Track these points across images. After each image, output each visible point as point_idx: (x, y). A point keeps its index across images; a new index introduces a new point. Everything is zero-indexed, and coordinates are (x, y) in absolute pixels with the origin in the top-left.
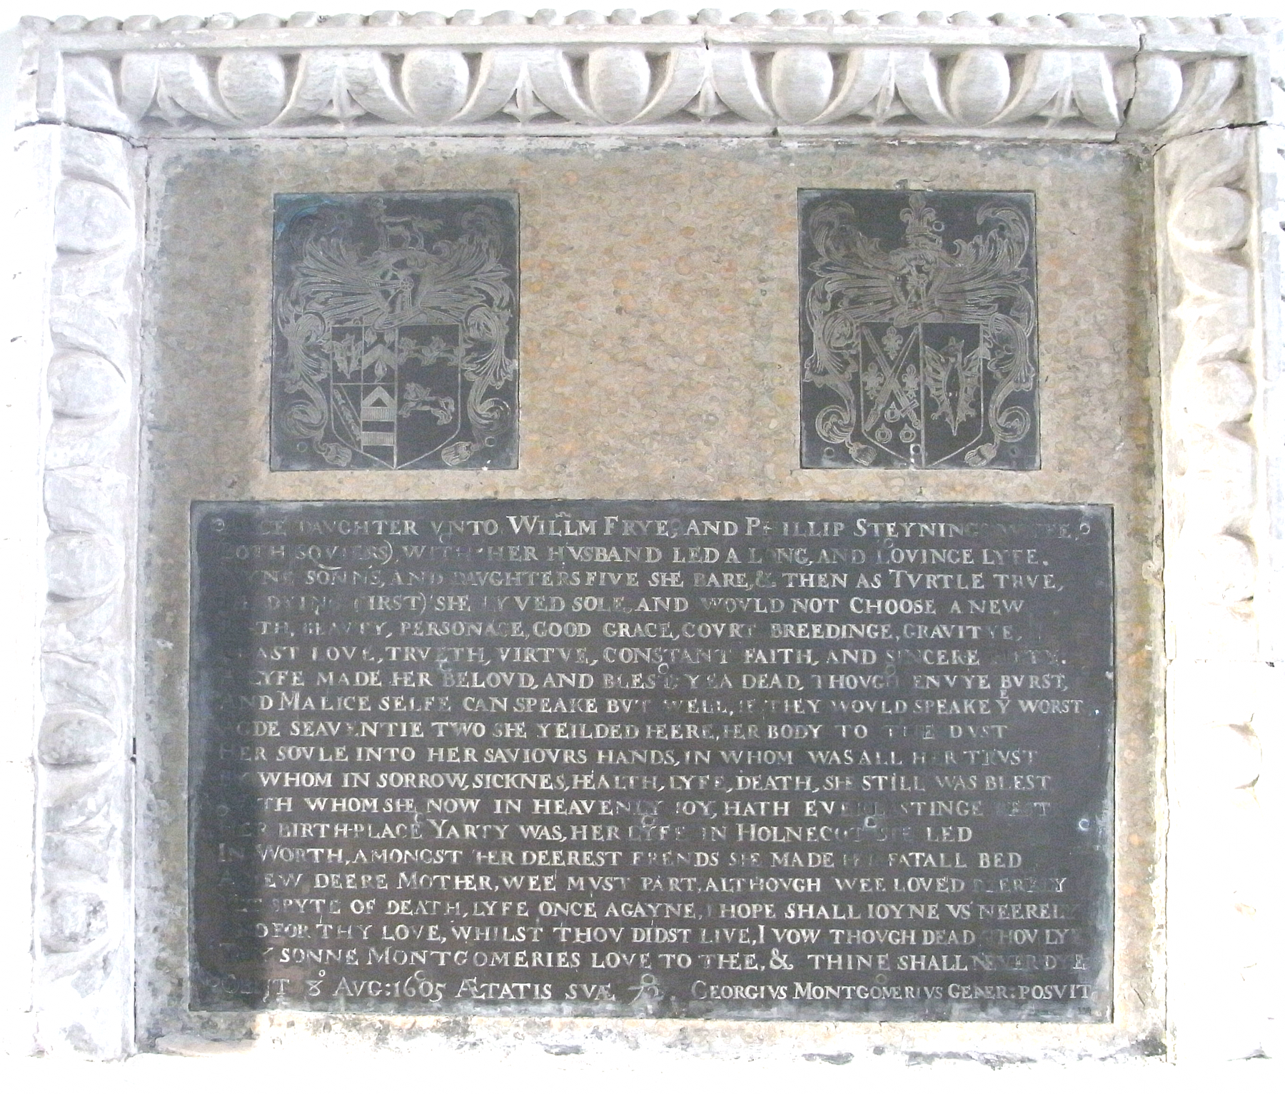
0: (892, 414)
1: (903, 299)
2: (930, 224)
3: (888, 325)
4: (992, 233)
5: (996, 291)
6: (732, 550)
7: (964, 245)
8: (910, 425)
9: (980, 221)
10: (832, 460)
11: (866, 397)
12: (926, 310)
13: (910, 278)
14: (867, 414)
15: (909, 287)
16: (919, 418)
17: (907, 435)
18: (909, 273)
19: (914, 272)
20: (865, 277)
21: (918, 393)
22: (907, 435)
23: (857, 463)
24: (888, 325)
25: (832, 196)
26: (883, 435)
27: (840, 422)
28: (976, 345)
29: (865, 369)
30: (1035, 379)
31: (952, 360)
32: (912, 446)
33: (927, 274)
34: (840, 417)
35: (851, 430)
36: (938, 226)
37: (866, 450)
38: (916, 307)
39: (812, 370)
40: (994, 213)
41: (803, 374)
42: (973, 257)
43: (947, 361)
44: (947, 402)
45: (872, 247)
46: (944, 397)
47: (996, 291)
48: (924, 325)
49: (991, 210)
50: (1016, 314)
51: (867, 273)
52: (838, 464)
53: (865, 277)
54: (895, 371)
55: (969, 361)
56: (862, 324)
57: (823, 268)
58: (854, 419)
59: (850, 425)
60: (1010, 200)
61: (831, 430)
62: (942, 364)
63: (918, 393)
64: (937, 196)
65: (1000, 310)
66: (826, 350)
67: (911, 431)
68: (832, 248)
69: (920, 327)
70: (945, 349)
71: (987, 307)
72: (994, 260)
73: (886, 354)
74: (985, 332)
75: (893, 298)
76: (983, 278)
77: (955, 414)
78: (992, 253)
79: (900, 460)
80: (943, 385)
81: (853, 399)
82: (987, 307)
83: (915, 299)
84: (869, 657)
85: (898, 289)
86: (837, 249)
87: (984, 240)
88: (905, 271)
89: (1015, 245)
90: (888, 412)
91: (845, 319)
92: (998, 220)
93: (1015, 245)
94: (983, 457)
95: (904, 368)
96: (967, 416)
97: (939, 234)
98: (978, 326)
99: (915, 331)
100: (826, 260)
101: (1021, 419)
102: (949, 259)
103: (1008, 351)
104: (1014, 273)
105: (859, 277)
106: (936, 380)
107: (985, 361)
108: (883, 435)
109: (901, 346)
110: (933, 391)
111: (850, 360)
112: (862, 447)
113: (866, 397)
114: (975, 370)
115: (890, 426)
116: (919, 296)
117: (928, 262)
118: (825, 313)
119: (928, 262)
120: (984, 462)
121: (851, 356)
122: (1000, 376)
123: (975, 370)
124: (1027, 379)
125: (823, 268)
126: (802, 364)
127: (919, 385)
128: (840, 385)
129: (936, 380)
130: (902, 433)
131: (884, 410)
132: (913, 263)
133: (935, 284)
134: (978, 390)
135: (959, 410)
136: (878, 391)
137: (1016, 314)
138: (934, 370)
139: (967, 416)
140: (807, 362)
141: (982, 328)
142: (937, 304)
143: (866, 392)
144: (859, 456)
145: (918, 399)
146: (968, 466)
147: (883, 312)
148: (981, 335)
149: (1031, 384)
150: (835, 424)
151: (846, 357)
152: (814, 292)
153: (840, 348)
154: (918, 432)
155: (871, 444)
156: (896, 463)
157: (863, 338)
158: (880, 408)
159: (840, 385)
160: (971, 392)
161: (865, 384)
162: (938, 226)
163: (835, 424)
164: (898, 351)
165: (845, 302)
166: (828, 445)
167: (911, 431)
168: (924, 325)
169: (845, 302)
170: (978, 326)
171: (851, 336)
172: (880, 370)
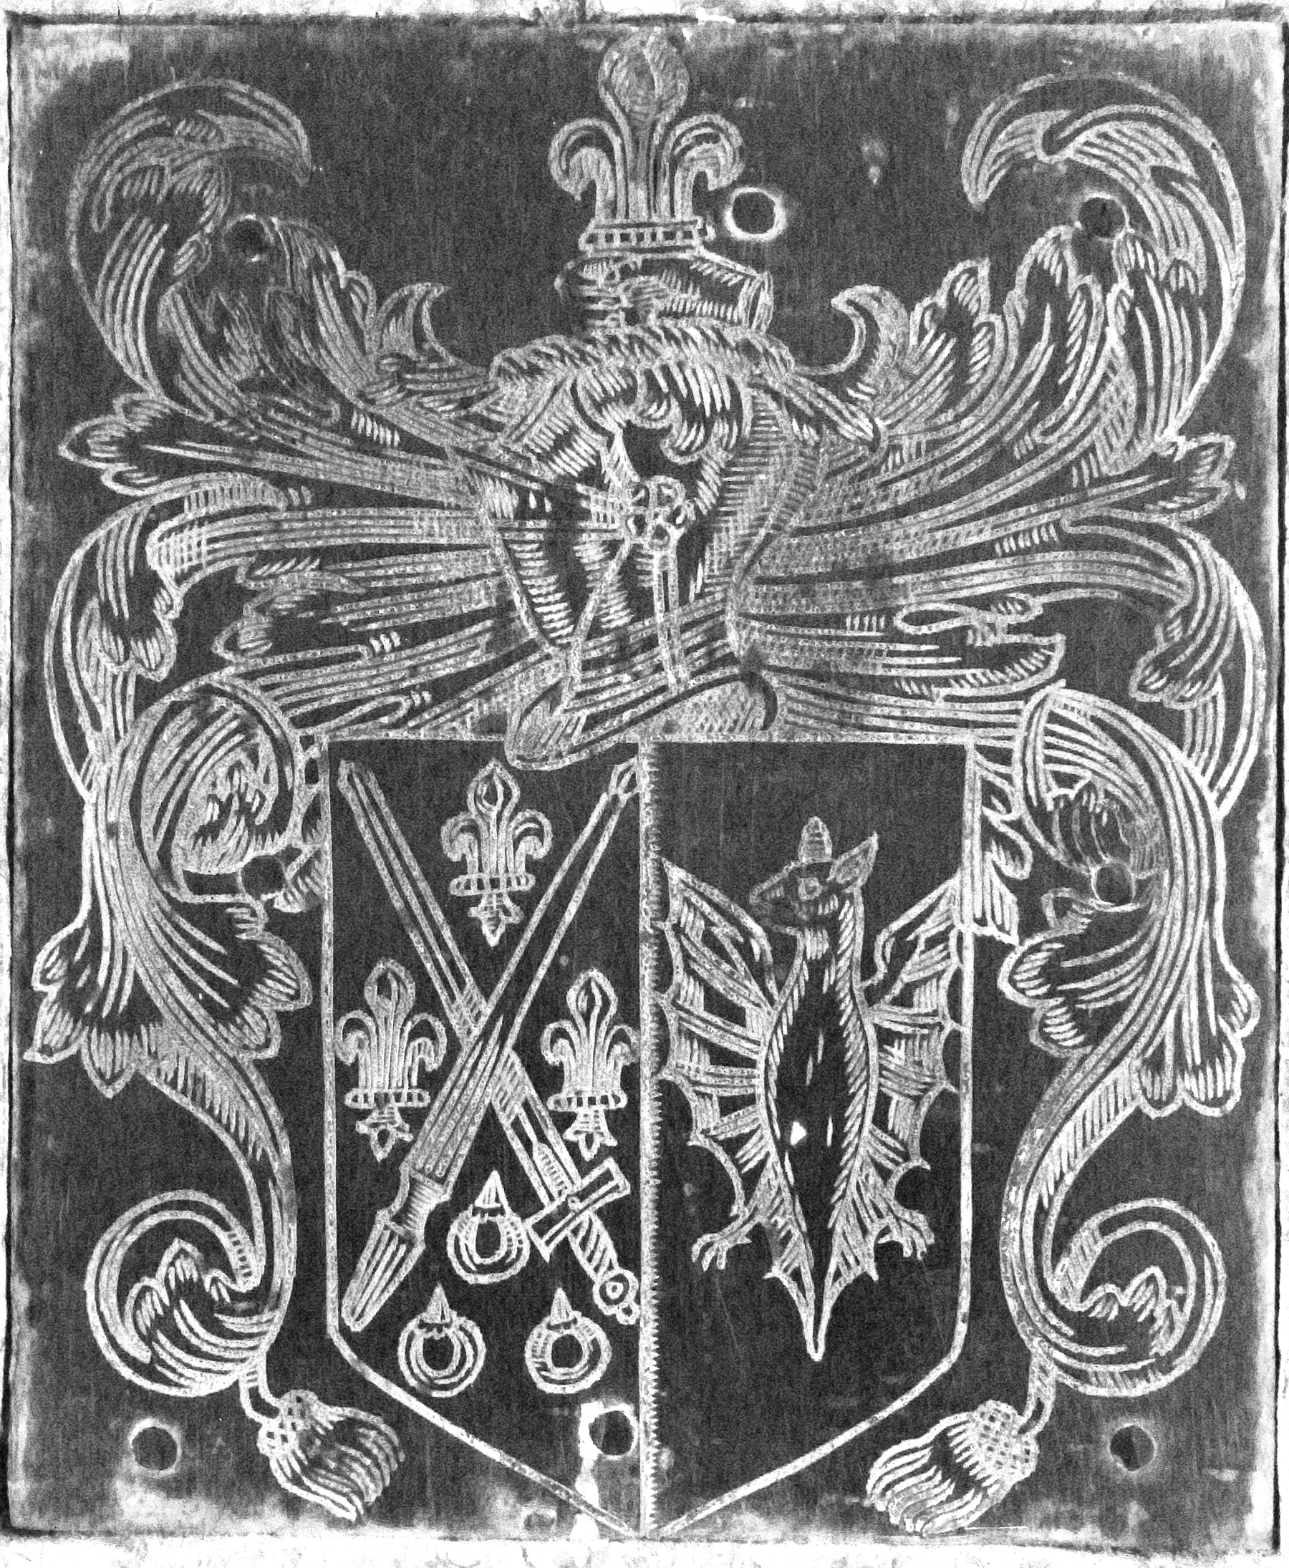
0: (488, 1239)
1: (556, 613)
2: (707, 202)
3: (474, 756)
4: (1042, 249)
5: (1059, 567)
6: (817, 1357)
7: (888, 315)
8: (581, 1301)
9: (978, 192)
10: (176, 1488)
11: (351, 1146)
12: (675, 676)
13: (594, 502)
14: (353, 1240)
15: (589, 551)
16: (629, 1258)
17: (566, 1352)
18: (593, 476)
19: (618, 456)
20: (356, 497)
21: (624, 1122)
22: (566, 1352)
23: (293, 1506)
24: (474, 756)
25: (190, 56)
26: (438, 1353)
27: (215, 1284)
28: (948, 865)
29: (349, 998)
30: (1255, 1044)
31: (812, 944)
32: (591, 1412)
33: (690, 475)
34: (213, 1254)
35: (272, 1323)
36: (754, 214)
37: (346, 1432)
38: (623, 655)
39: (72, 1001)
40: (1053, 142)
41: (23, 1025)
42: (937, 385)
43: (785, 950)
44: (778, 1176)
45: (398, 336)
46: (761, 1147)
47: (1059, 567)
48: (668, 756)
49: (1042, 122)
50: (1156, 690)
51: (368, 472)
52: (199, 1510)
53: (356, 497)
54: (506, 1009)
55: (903, 950)
56: (338, 752)
57: (130, 447)
58: (285, 1273)
59: (261, 1297)
60: (1144, 63)
61: (164, 1323)
62: (758, 972)
63: (624, 1122)
64: (751, 51)
65: (1075, 674)
66: (141, 887)
67: (588, 1332)
68: (191, 343)
69: (643, 767)
70: (772, 886)
71: (1000, 658)
72: (1051, 392)
73: (458, 910)
74: (990, 793)
75: (504, 609)
76: (987, 495)
77: (820, 1240)
78: (1042, 353)
79: (523, 1490)
80: (760, 1083)
81: (282, 1159)
82: (1000, 658)
83: (618, 616)
84: (269, 982)
85: (535, 563)
86: (217, 347)
87: (1001, 284)
88: (570, 463)
89: (1164, 308)
90: (464, 1231)
91: (250, 722)
92: (1080, 175)
93: (1164, 308)
94: (964, 1481)
95: (560, 978)
96: (887, 1253)
97: (754, 257)
98: (956, 755)
99: (616, 788)
100: (154, 400)
101: (1175, 1274)
102: (807, 393)
103: (1114, 889)
104: (1156, 465)
105: (329, 495)
106: (721, 1056)
107: (990, 953)
108: (438, 1353)
109: (536, 868)
110: (706, 1117)
111: (276, 952)
112: (328, 1415)
113: (351, 1146)
114: (932, 999)
115: (463, 1299)
116: (639, 603)
117: (693, 414)
118: (148, 693)
119: (693, 414)
120: (973, 1505)
121: (278, 923)
122: (1063, 1031)
123: (932, 999)
124: (1213, 1048)
125: (130, 447)
126: (21, 974)
127: (630, 1079)
128: (221, 1089)
129: (721, 1056)
130: (540, 1341)
131: (439, 1222)
132: (614, 419)
133: (725, 542)
134: (949, 1101)
135: (840, 1221)
136: (415, 1118)
137: (1156, 690)
138: (716, 1003)
139: (887, 1253)
140: (47, 956)
141: (976, 768)
142: (734, 640)
143: (348, 1117)
144: (313, 1466)
145: (628, 1158)
146: (884, 1528)
147: (446, 690)
148: (973, 811)
149: (1231, 1077)
150: (188, 1291)
151: (254, 930)
152: (86, 588)
153: (223, 883)
154: (624, 1339)
155: (380, 1403)
156: (501, 1502)
157: (346, 839)
158: (432, 1198)
159: (221, 1089)
160: (904, 1120)
161: (348, 1076)
162: (754, 214)
163: (188, 1291)
164: (526, 902)
165: (251, 630)
166: (153, 1404)
167: (588, 1332)
168: (668, 756)
169: (251, 630)
170: (956, 755)
171: (278, 822)
172: (427, 1001)
